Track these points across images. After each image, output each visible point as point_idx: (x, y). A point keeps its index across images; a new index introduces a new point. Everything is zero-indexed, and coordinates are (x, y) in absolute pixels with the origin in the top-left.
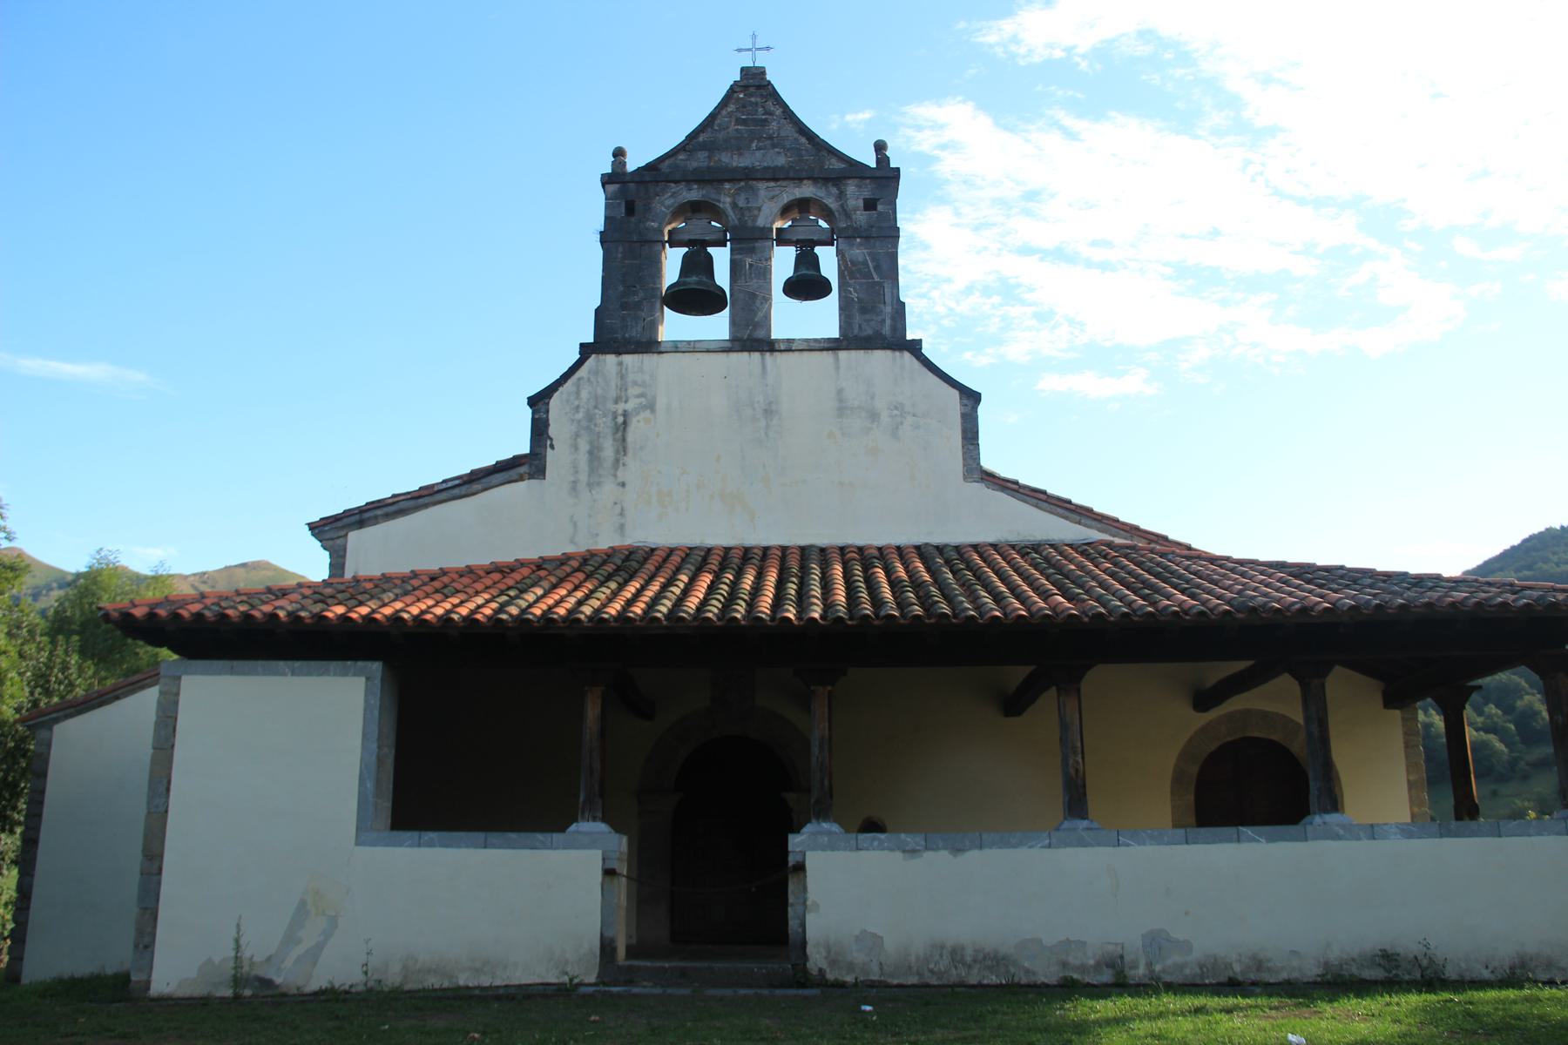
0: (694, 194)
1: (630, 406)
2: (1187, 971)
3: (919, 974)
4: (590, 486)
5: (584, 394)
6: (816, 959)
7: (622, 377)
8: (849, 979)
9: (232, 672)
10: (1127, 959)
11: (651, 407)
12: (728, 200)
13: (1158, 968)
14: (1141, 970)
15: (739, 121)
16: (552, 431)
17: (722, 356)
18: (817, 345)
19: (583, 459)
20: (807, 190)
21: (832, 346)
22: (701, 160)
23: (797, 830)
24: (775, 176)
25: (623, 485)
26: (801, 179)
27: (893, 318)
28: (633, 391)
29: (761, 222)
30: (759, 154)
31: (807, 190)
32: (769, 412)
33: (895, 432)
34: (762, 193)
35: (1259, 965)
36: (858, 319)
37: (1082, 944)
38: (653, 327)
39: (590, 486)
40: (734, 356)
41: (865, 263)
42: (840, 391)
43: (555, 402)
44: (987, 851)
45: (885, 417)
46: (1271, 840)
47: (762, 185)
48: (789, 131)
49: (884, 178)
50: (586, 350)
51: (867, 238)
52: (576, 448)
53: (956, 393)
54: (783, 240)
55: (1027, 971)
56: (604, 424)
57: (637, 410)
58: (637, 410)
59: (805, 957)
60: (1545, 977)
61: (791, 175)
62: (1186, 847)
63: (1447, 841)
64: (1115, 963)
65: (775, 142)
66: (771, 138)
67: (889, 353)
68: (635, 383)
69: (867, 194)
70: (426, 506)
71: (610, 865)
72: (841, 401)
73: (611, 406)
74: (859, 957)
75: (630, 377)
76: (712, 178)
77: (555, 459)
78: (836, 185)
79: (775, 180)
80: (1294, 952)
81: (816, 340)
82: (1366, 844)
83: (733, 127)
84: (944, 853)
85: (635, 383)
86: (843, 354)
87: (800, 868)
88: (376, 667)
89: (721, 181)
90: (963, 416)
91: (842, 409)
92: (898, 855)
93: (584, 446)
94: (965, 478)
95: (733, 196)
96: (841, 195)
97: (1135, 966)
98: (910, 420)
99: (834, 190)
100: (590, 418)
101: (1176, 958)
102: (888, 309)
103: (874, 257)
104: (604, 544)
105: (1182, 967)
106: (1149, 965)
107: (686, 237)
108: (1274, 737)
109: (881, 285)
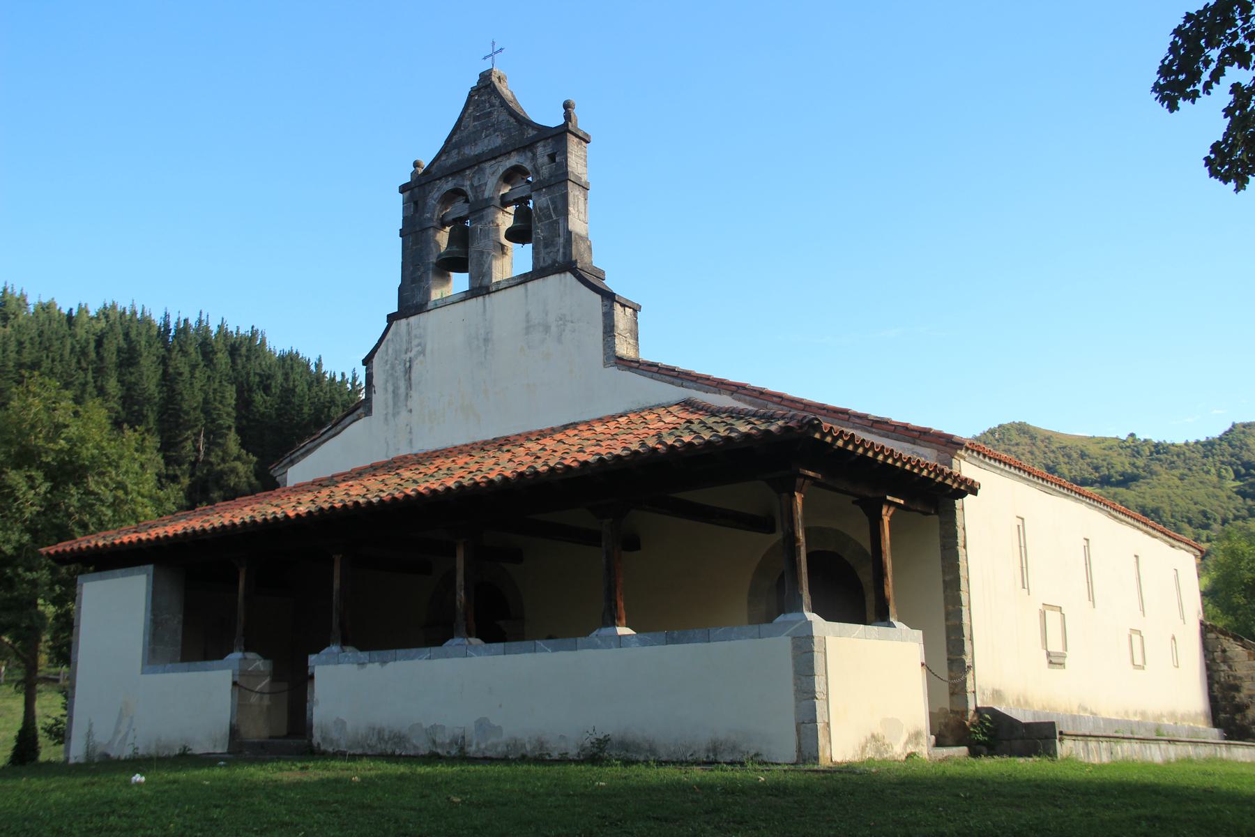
0: (448, 185)
1: (412, 354)
2: (499, 749)
3: (363, 747)
4: (394, 415)
5: (390, 351)
6: (317, 738)
7: (409, 333)
8: (330, 750)
9: (102, 578)
10: (467, 739)
11: (423, 352)
12: (468, 183)
13: (483, 746)
14: (473, 748)
15: (476, 119)
16: (375, 381)
17: (462, 304)
18: (512, 282)
19: (390, 396)
20: (514, 160)
21: (524, 279)
22: (454, 157)
23: (317, 652)
24: (495, 155)
25: (411, 411)
26: (509, 153)
27: (564, 247)
28: (415, 342)
29: (487, 195)
30: (486, 141)
31: (514, 160)
32: (486, 340)
33: (559, 340)
34: (488, 171)
35: (541, 744)
36: (543, 253)
37: (443, 728)
38: (427, 293)
39: (394, 415)
40: (468, 302)
41: (548, 207)
42: (527, 315)
43: (376, 360)
44: (398, 662)
45: (554, 329)
46: (555, 650)
47: (487, 165)
48: (504, 116)
49: (558, 138)
50: (391, 318)
51: (549, 187)
52: (386, 390)
53: (598, 297)
54: (505, 202)
55: (415, 747)
56: (400, 369)
57: (416, 356)
58: (416, 356)
59: (312, 736)
60: (728, 759)
61: (503, 151)
62: (502, 657)
63: (672, 648)
64: (460, 743)
65: (496, 128)
66: (493, 125)
67: (557, 276)
68: (416, 336)
69: (549, 151)
70: (319, 445)
71: (237, 679)
72: (528, 321)
73: (403, 356)
74: (334, 735)
75: (414, 332)
76: (457, 171)
77: (377, 399)
78: (531, 151)
79: (495, 158)
80: (562, 737)
81: (513, 278)
82: (615, 650)
83: (472, 124)
84: (377, 664)
85: (416, 336)
86: (530, 284)
87: (312, 677)
88: (151, 567)
89: (464, 170)
90: (604, 314)
91: (528, 329)
92: (355, 666)
93: (390, 388)
94: (605, 365)
95: (471, 179)
96: (534, 158)
97: (470, 745)
98: (570, 325)
99: (530, 154)
100: (393, 367)
101: (493, 740)
102: (561, 240)
103: (553, 202)
104: (402, 453)
105: (495, 746)
106: (478, 744)
107: (450, 218)
108: (830, 549)
109: (557, 222)
